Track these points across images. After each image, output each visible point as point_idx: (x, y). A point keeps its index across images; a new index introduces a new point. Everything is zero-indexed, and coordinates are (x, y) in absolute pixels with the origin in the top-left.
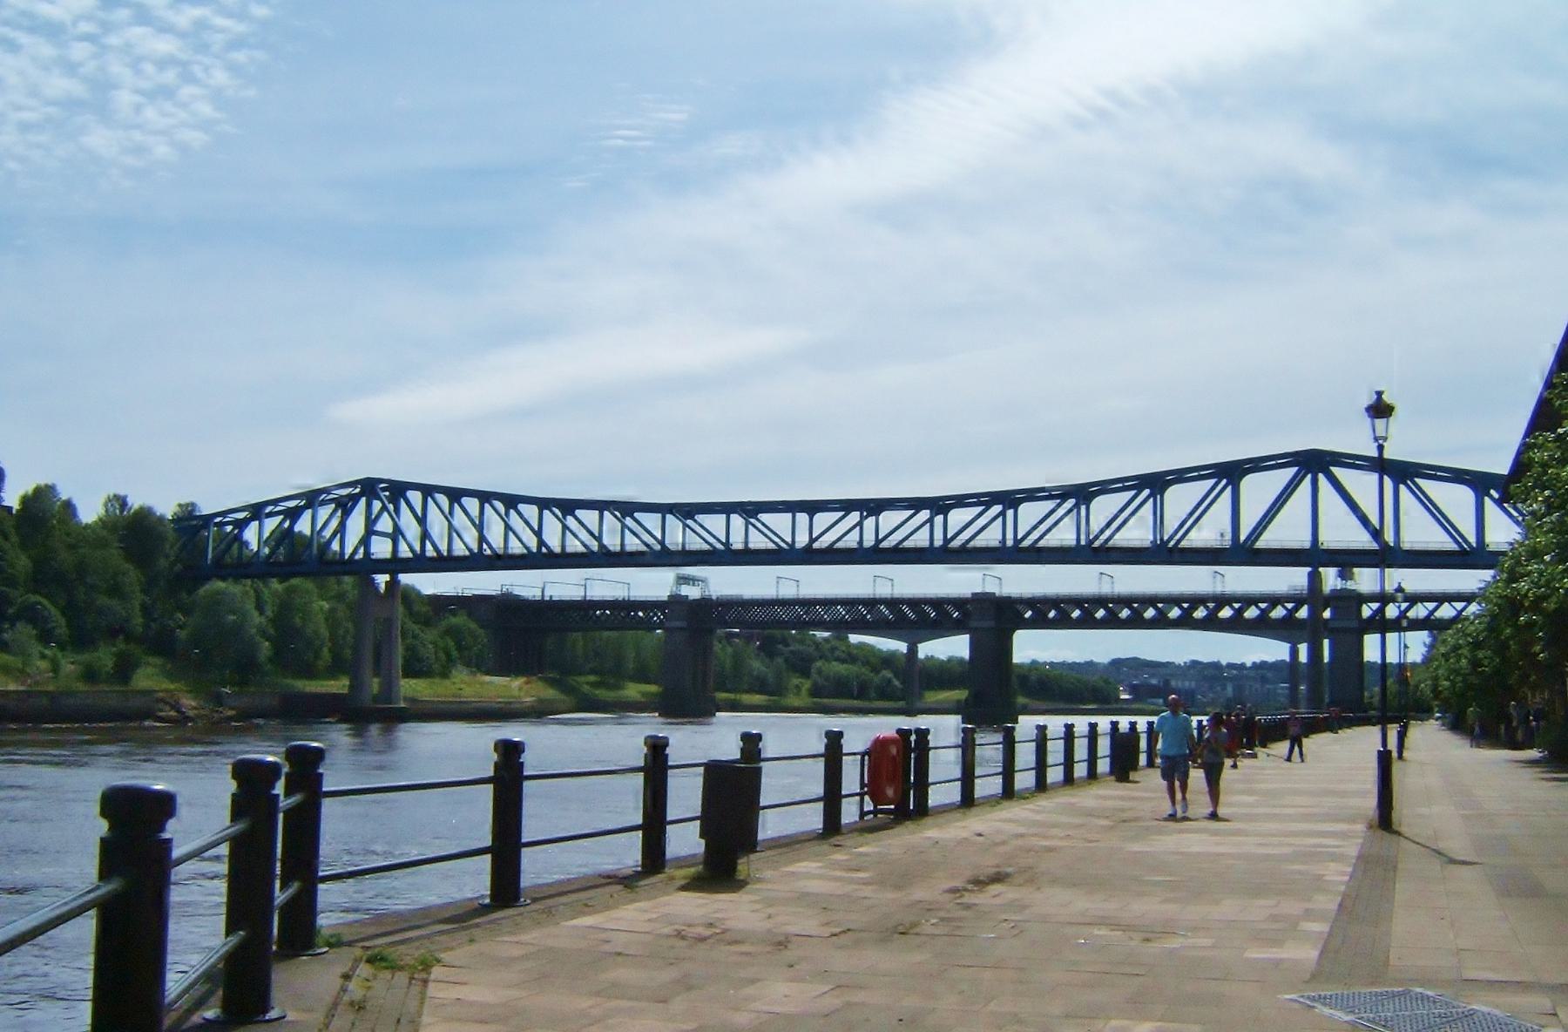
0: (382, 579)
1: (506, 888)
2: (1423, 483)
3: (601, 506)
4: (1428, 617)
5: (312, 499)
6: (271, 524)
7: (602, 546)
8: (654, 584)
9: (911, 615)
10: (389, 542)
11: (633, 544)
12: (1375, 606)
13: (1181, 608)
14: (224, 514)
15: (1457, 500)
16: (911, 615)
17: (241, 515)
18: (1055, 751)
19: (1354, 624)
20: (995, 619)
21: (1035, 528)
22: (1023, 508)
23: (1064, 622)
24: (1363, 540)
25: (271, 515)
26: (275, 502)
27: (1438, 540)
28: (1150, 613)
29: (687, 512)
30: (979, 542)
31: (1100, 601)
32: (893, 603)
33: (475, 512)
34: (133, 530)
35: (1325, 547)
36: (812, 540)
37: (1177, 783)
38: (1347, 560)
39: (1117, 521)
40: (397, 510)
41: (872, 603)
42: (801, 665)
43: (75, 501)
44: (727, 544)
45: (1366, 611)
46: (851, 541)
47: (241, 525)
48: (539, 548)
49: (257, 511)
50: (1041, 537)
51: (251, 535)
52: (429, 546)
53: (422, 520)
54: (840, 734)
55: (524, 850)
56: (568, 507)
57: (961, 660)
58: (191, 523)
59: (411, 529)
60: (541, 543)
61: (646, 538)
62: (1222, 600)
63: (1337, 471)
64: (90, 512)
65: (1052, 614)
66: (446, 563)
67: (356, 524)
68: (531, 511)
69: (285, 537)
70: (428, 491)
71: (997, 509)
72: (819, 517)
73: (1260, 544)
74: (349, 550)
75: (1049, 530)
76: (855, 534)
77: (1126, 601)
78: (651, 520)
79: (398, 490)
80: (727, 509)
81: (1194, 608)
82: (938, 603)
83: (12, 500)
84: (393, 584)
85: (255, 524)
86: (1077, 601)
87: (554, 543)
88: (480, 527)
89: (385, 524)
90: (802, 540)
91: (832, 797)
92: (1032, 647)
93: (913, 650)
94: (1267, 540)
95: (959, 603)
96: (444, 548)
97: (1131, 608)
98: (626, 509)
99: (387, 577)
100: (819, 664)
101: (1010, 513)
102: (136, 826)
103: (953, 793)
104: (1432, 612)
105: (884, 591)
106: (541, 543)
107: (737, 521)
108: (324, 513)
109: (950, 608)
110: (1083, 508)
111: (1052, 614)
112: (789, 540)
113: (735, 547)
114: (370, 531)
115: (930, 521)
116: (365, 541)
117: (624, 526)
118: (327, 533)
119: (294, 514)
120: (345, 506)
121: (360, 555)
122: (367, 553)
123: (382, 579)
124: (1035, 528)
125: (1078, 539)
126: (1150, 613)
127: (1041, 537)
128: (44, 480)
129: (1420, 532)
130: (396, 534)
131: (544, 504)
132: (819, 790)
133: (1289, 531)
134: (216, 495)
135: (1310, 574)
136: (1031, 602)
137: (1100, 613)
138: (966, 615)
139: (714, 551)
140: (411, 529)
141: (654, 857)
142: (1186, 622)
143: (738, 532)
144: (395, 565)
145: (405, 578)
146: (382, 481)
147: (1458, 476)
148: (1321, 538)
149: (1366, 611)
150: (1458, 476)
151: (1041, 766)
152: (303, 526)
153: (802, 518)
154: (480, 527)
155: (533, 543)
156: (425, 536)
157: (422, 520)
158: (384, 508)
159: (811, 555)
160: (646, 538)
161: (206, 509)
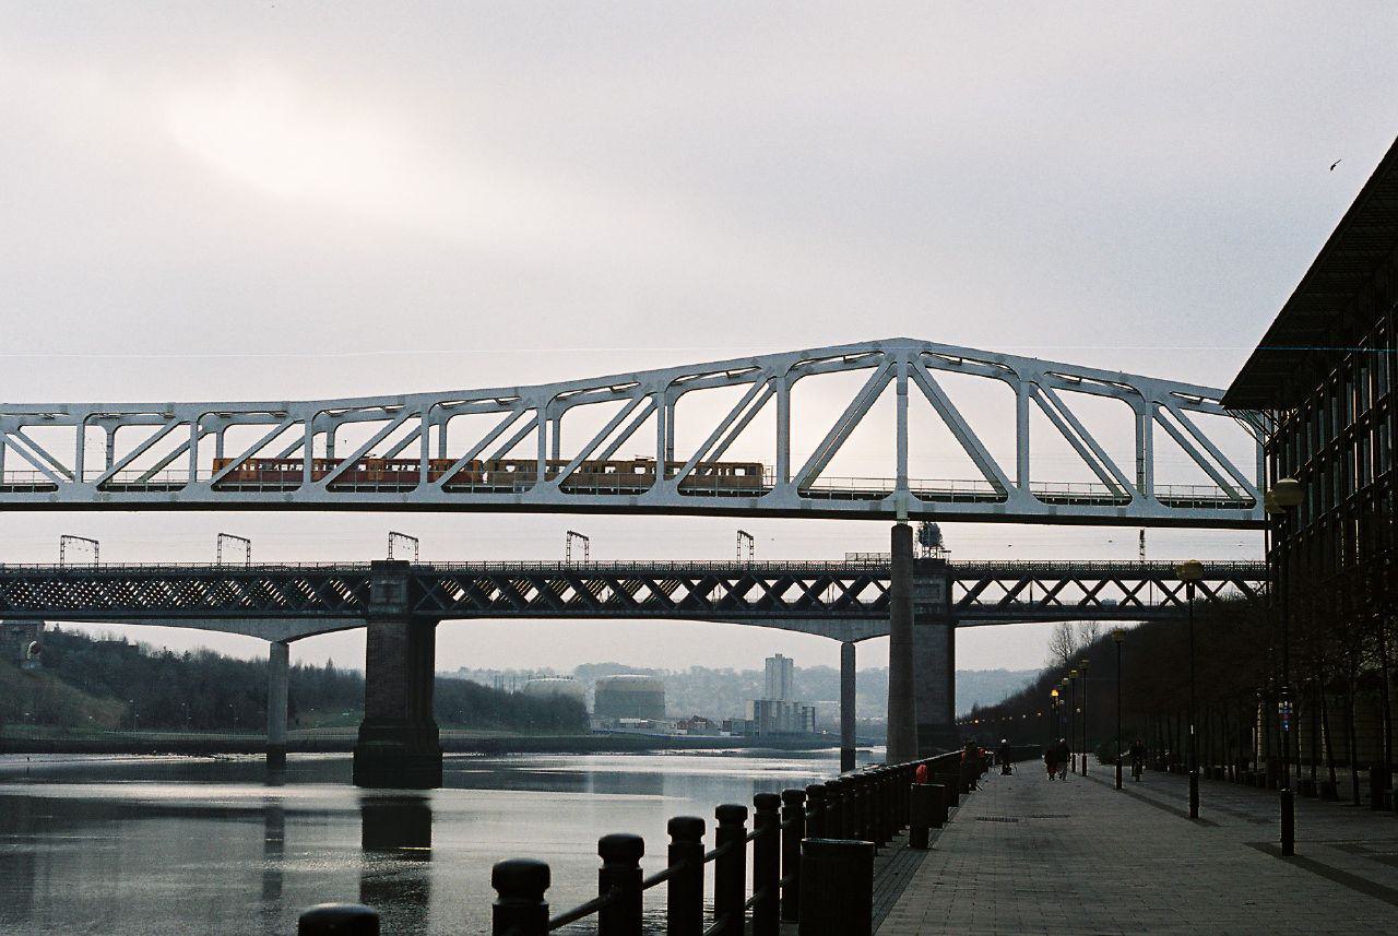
2: (1067, 397)
4: (1006, 600)
9: (278, 597)
12: (971, 584)
13: (689, 586)
16: (278, 597)
20: (408, 602)
22: (455, 423)
23: (514, 607)
24: (964, 476)
27: (1080, 480)
28: (643, 594)
31: (570, 575)
32: (250, 576)
37: (656, 900)
38: (940, 508)
41: (215, 576)
45: (958, 593)
46: (178, 472)
57: (354, 674)
62: (749, 575)
63: (942, 378)
65: (495, 595)
73: (820, 483)
77: (609, 575)
81: (708, 586)
82: (319, 577)
86: (537, 576)
92: (466, 649)
95: (354, 577)
97: (614, 586)
101: (434, 431)
102: (1350, 800)
104: (1051, 595)
105: (234, 557)
109: (338, 585)
126: (643, 594)
129: (1058, 469)
133: (863, 463)
135: (894, 529)
137: (568, 595)
138: (363, 594)
142: (695, 609)
147: (998, 367)
149: (958, 593)
150: (998, 367)
153: (96, 434)
159: (112, 497)
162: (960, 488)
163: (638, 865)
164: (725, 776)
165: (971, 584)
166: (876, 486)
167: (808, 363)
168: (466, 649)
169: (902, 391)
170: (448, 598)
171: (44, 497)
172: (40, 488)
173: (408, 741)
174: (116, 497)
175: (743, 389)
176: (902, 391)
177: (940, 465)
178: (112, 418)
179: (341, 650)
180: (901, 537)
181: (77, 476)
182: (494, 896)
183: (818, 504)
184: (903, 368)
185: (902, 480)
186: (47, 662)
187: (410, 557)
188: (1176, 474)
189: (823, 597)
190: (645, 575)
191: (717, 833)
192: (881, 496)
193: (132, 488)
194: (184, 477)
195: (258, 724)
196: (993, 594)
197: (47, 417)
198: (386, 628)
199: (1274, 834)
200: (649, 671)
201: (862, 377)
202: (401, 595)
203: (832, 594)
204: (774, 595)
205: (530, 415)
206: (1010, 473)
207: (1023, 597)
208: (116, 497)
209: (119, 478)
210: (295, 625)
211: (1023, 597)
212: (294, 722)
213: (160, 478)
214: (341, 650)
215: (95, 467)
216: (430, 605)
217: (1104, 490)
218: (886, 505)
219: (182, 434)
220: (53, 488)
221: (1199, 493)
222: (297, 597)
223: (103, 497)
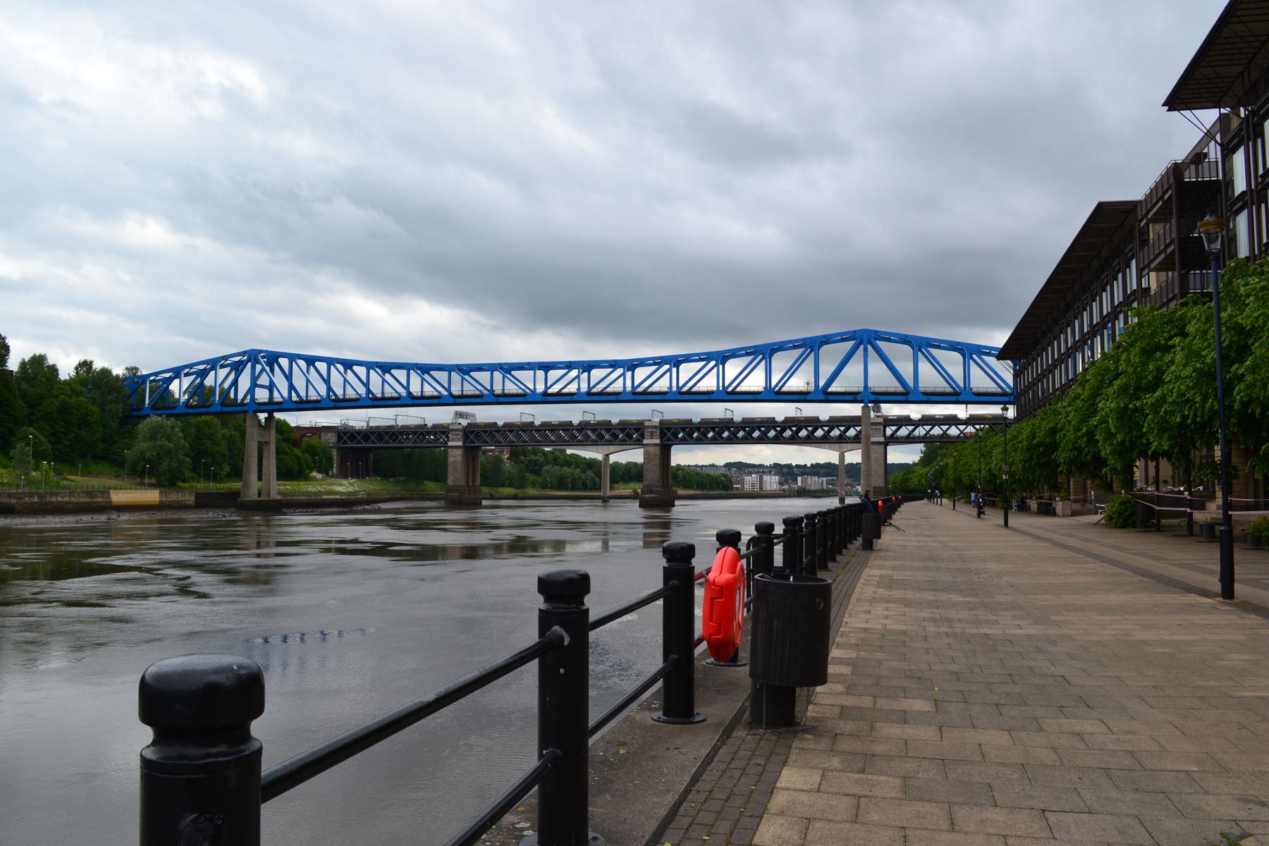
0: (262, 416)
2: (932, 351)
3: (408, 367)
5: (214, 364)
6: (187, 382)
7: (409, 393)
10: (267, 392)
11: (428, 391)
12: (894, 428)
14: (156, 374)
15: (953, 362)
17: (167, 375)
19: (882, 439)
22: (683, 366)
26: (190, 366)
27: (939, 384)
29: (465, 370)
30: (655, 388)
34: (91, 379)
35: (975, 390)
36: (547, 388)
39: (700, 375)
40: (272, 371)
42: (535, 468)
43: (59, 367)
44: (492, 391)
45: (889, 431)
46: (572, 388)
47: (169, 381)
48: (328, 395)
49: (177, 373)
51: (174, 386)
52: (294, 394)
53: (289, 377)
56: (386, 368)
58: (134, 380)
60: (329, 389)
63: (882, 344)
64: (66, 368)
65: (680, 435)
66: (305, 405)
67: (244, 382)
68: (361, 371)
69: (198, 390)
70: (292, 358)
72: (551, 373)
73: (830, 390)
74: (240, 397)
78: (442, 376)
79: (273, 358)
80: (491, 368)
83: (13, 364)
84: (270, 419)
85: (177, 381)
87: (376, 390)
88: (327, 381)
89: (264, 380)
90: (540, 388)
92: (683, 456)
93: (842, 458)
94: (834, 388)
96: (303, 394)
98: (424, 369)
99: (266, 415)
100: (547, 468)
101: (674, 370)
106: (369, 391)
107: (498, 375)
108: (222, 373)
110: (674, 370)
113: (455, 393)
114: (254, 384)
115: (623, 375)
116: (251, 391)
117: (384, 380)
118: (226, 385)
119: (203, 374)
120: (238, 368)
121: (248, 400)
122: (253, 399)
123: (262, 416)
128: (39, 351)
129: (929, 378)
130: (271, 387)
131: (369, 366)
133: (851, 379)
139: (481, 396)
143: (500, 383)
144: (272, 406)
145: (277, 415)
146: (261, 351)
147: (905, 340)
148: (870, 385)
150: (905, 340)
152: (209, 381)
153: (541, 373)
154: (327, 381)
155: (323, 390)
157: (289, 377)
158: (263, 370)
159: (547, 398)
161: (144, 372)
162: (890, 390)
163: (247, 737)
164: (345, 434)
165: (894, 428)
166: (855, 390)
167: (827, 340)
168: (683, 456)
169: (866, 350)
173: (662, 489)
174: (550, 399)
175: (801, 350)
176: (866, 350)
177: (880, 378)
178: (547, 367)
179: (634, 456)
180: (865, 409)
182: (539, 602)
183: (550, 399)
184: (865, 340)
185: (866, 387)
188: (980, 381)
189: (848, 434)
191: (541, 618)
192: (858, 393)
196: (904, 432)
198: (652, 449)
199: (1002, 522)
201: (850, 344)
203: (836, 433)
204: (720, 434)
205: (713, 363)
206: (911, 383)
207: (916, 433)
209: (550, 391)
210: (612, 448)
211: (916, 433)
214: (634, 456)
216: (669, 439)
217: (950, 390)
218: (859, 398)
219: (574, 373)
221: (990, 390)
223: (544, 399)
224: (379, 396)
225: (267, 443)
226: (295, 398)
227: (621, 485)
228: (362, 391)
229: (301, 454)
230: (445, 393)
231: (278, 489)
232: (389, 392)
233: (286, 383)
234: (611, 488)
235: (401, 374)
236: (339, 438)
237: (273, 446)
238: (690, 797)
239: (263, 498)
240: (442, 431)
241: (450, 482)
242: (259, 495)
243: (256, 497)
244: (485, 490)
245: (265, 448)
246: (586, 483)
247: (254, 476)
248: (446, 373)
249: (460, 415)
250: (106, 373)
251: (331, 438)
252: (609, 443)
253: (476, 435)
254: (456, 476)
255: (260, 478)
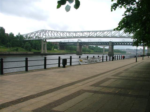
1: (27, 70)
5: (37, 32)
7: (67, 36)
8: (76, 40)
11: (83, 35)
18: (119, 57)
21: (121, 34)
25: (33, 34)
28: (128, 44)
30: (115, 35)
31: (123, 42)
33: (60, 33)
46: (101, 35)
50: (107, 35)
52: (52, 36)
53: (54, 34)
54: (71, 57)
55: (28, 67)
59: (47, 34)
61: (78, 35)
71: (109, 32)
75: (116, 34)
76: (90, 34)
86: (121, 42)
88: (60, 35)
89: (45, 34)
91: (59, 63)
92: (116, 47)
95: (108, 42)
96: (51, 37)
99: (45, 40)
101: (119, 32)
103: (109, 60)
105: (100, 41)
106: (60, 36)
108: (38, 33)
111: (120, 44)
112: (86, 35)
114: (43, 35)
115: (102, 33)
124: (121, 34)
125: (118, 35)
127: (107, 35)
132: (58, 63)
134: (23, 33)
136: (116, 43)
140: (47, 34)
141: (59, 66)
151: (120, 58)
153: (88, 33)
154: (60, 35)
155: (59, 36)
156: (54, 35)
157: (54, 34)
159: (89, 37)
160: (78, 35)
164: (61, 43)
168: (116, 47)
170: (114, 44)
171: (85, 37)
172: (85, 37)
178: (89, 32)
179: (107, 47)
181: (87, 36)
186: (89, 48)
187: (112, 41)
190: (128, 42)
193: (98, 36)
194: (101, 36)
195: (102, 52)
197: (85, 32)
198: (110, 46)
200: (124, 49)
202: (111, 44)
205: (109, 32)
208: (89, 37)
209: (105, 36)
210: (105, 46)
212: (105, 52)
213: (100, 36)
214: (107, 47)
215: (88, 35)
219: (101, 33)
220: (85, 37)
222: (102, 44)
223: (89, 37)
224: (62, 37)
225: (45, 44)
226: (49, 37)
227: (107, 52)
228: (66, 36)
229: (51, 46)
230: (79, 36)
231: (46, 52)
232: (70, 36)
233: (49, 34)
234: (105, 52)
235: (72, 33)
236: (60, 44)
237: (46, 45)
238: (15, 72)
239: (45, 53)
240: (75, 43)
241: (77, 51)
242: (44, 53)
243: (43, 53)
244: (83, 52)
245: (45, 45)
246: (100, 51)
247: (43, 50)
248: (73, 33)
249: (79, 40)
250: (12, 35)
251: (58, 44)
252: (105, 45)
253: (81, 44)
254: (78, 50)
255: (44, 50)
